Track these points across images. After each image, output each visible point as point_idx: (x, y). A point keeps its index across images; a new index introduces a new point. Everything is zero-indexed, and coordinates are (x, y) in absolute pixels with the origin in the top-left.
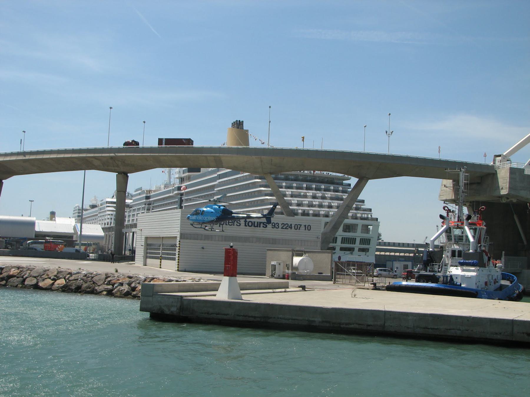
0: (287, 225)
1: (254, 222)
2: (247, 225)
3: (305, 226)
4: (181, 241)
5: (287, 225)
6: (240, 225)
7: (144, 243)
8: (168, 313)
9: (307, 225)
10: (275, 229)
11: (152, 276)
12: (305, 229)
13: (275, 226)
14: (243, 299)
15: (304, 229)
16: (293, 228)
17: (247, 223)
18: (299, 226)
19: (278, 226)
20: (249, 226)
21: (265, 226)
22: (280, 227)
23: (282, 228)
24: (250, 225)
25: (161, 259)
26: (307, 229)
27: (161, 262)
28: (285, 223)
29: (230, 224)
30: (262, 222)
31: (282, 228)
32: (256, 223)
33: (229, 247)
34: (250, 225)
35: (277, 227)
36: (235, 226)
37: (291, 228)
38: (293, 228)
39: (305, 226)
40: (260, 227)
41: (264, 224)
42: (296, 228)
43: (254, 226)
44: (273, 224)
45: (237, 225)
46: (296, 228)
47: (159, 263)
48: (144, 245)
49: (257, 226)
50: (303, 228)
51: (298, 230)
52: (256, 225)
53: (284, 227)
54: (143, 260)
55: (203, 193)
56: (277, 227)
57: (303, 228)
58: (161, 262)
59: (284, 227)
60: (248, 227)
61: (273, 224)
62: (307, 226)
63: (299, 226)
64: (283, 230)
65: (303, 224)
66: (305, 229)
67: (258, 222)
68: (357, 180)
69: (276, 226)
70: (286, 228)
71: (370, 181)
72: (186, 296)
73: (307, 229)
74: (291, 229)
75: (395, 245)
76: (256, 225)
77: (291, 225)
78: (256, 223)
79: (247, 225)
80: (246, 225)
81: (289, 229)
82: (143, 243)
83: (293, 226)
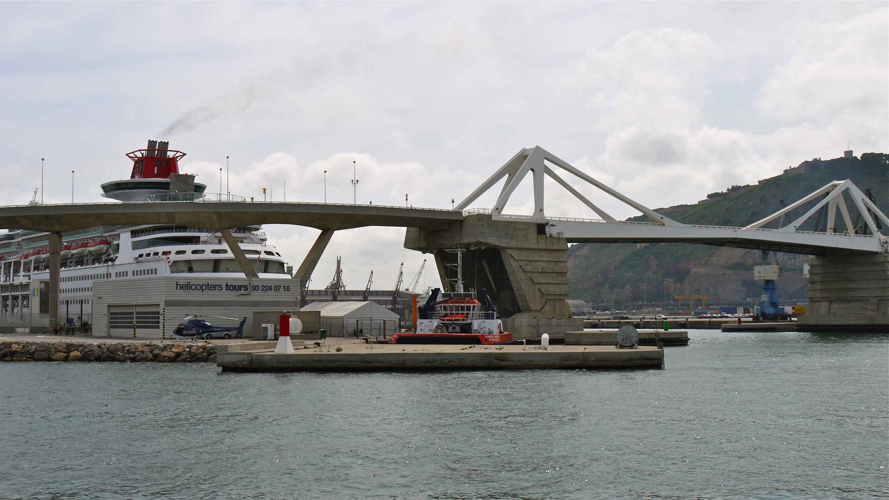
0: (267, 287)
1: (235, 286)
2: (228, 289)
3: (284, 287)
4: (166, 308)
5: (267, 287)
6: (222, 289)
7: (106, 312)
8: (241, 366)
9: (286, 285)
10: (256, 291)
11: (850, 286)
12: (285, 290)
13: (255, 288)
14: (532, 309)
15: (283, 289)
16: (273, 289)
17: (209, 286)
18: (278, 287)
19: (258, 288)
20: (231, 290)
21: (245, 289)
22: (260, 289)
23: (262, 290)
24: (231, 289)
25: (135, 328)
26: (286, 289)
27: (135, 331)
28: (265, 285)
29: (212, 289)
30: (243, 286)
31: (262, 290)
32: (237, 286)
33: (282, 314)
34: (231, 289)
35: (258, 289)
36: (217, 291)
37: (271, 290)
38: (273, 289)
39: (284, 287)
40: (241, 290)
41: (244, 287)
42: (276, 289)
43: (236, 290)
44: (254, 287)
45: (219, 289)
46: (276, 289)
47: (133, 333)
48: (106, 314)
49: (238, 290)
50: (282, 289)
51: (277, 292)
52: (237, 289)
53: (265, 289)
54: (106, 330)
55: (609, 332)
56: (258, 289)
57: (282, 289)
58: (135, 331)
59: (265, 289)
60: (229, 291)
61: (254, 287)
62: (286, 287)
63: (278, 287)
64: (263, 292)
65: (283, 285)
66: (285, 290)
67: (239, 286)
68: (319, 232)
69: (256, 288)
70: (266, 290)
71: (335, 232)
72: (253, 353)
73: (286, 289)
74: (227, 284)
75: (321, 294)
76: (237, 289)
77: (271, 286)
78: (237, 286)
79: (228, 289)
80: (227, 290)
81: (269, 291)
82: (106, 312)
83: (273, 287)
